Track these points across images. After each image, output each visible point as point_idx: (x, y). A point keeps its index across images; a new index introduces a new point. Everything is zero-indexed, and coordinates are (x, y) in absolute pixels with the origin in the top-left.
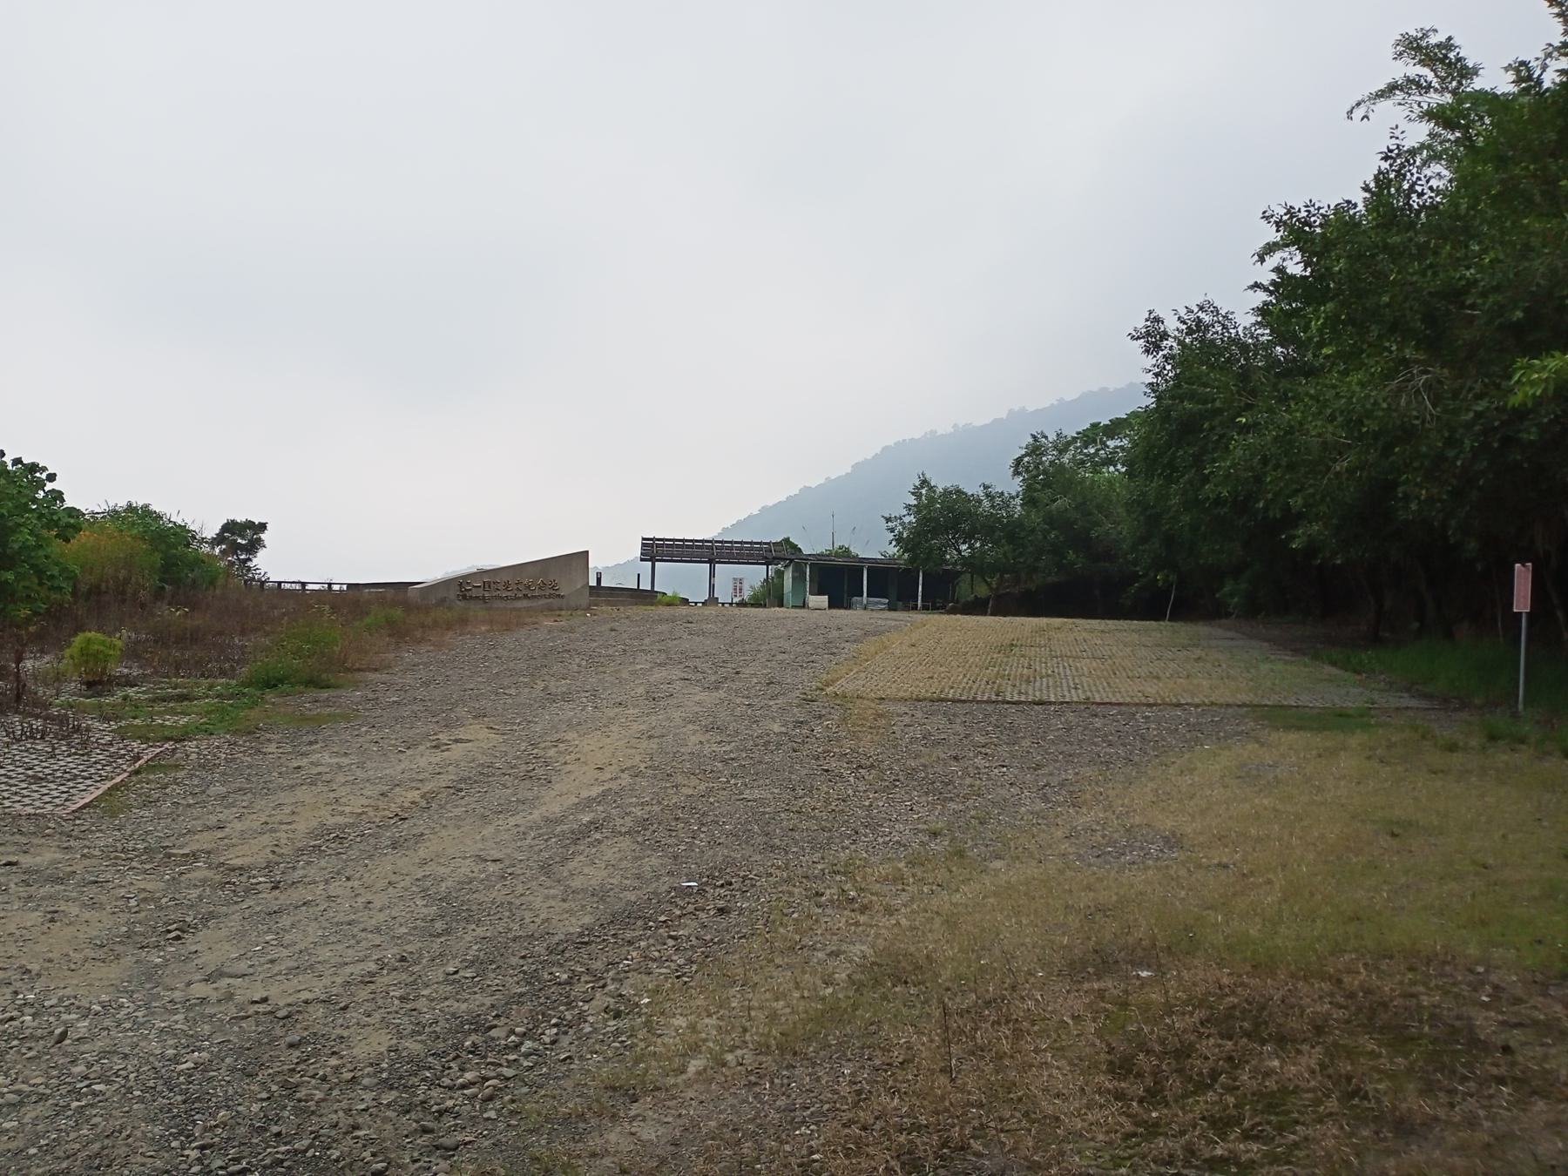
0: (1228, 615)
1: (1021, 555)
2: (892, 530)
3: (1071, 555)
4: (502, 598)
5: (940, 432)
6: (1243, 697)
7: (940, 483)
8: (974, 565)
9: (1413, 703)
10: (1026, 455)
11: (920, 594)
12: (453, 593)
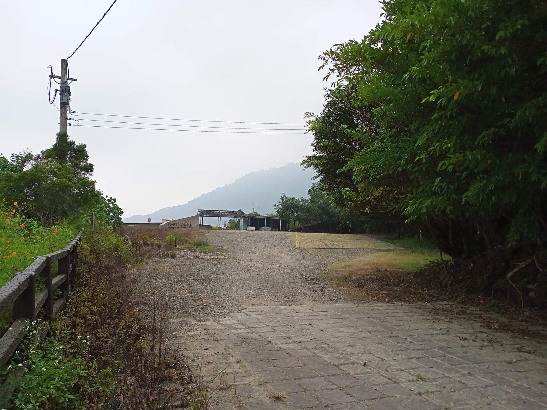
0: (365, 232)
1: (311, 216)
6: (374, 248)
7: (289, 196)
8: (298, 219)
10: (311, 189)
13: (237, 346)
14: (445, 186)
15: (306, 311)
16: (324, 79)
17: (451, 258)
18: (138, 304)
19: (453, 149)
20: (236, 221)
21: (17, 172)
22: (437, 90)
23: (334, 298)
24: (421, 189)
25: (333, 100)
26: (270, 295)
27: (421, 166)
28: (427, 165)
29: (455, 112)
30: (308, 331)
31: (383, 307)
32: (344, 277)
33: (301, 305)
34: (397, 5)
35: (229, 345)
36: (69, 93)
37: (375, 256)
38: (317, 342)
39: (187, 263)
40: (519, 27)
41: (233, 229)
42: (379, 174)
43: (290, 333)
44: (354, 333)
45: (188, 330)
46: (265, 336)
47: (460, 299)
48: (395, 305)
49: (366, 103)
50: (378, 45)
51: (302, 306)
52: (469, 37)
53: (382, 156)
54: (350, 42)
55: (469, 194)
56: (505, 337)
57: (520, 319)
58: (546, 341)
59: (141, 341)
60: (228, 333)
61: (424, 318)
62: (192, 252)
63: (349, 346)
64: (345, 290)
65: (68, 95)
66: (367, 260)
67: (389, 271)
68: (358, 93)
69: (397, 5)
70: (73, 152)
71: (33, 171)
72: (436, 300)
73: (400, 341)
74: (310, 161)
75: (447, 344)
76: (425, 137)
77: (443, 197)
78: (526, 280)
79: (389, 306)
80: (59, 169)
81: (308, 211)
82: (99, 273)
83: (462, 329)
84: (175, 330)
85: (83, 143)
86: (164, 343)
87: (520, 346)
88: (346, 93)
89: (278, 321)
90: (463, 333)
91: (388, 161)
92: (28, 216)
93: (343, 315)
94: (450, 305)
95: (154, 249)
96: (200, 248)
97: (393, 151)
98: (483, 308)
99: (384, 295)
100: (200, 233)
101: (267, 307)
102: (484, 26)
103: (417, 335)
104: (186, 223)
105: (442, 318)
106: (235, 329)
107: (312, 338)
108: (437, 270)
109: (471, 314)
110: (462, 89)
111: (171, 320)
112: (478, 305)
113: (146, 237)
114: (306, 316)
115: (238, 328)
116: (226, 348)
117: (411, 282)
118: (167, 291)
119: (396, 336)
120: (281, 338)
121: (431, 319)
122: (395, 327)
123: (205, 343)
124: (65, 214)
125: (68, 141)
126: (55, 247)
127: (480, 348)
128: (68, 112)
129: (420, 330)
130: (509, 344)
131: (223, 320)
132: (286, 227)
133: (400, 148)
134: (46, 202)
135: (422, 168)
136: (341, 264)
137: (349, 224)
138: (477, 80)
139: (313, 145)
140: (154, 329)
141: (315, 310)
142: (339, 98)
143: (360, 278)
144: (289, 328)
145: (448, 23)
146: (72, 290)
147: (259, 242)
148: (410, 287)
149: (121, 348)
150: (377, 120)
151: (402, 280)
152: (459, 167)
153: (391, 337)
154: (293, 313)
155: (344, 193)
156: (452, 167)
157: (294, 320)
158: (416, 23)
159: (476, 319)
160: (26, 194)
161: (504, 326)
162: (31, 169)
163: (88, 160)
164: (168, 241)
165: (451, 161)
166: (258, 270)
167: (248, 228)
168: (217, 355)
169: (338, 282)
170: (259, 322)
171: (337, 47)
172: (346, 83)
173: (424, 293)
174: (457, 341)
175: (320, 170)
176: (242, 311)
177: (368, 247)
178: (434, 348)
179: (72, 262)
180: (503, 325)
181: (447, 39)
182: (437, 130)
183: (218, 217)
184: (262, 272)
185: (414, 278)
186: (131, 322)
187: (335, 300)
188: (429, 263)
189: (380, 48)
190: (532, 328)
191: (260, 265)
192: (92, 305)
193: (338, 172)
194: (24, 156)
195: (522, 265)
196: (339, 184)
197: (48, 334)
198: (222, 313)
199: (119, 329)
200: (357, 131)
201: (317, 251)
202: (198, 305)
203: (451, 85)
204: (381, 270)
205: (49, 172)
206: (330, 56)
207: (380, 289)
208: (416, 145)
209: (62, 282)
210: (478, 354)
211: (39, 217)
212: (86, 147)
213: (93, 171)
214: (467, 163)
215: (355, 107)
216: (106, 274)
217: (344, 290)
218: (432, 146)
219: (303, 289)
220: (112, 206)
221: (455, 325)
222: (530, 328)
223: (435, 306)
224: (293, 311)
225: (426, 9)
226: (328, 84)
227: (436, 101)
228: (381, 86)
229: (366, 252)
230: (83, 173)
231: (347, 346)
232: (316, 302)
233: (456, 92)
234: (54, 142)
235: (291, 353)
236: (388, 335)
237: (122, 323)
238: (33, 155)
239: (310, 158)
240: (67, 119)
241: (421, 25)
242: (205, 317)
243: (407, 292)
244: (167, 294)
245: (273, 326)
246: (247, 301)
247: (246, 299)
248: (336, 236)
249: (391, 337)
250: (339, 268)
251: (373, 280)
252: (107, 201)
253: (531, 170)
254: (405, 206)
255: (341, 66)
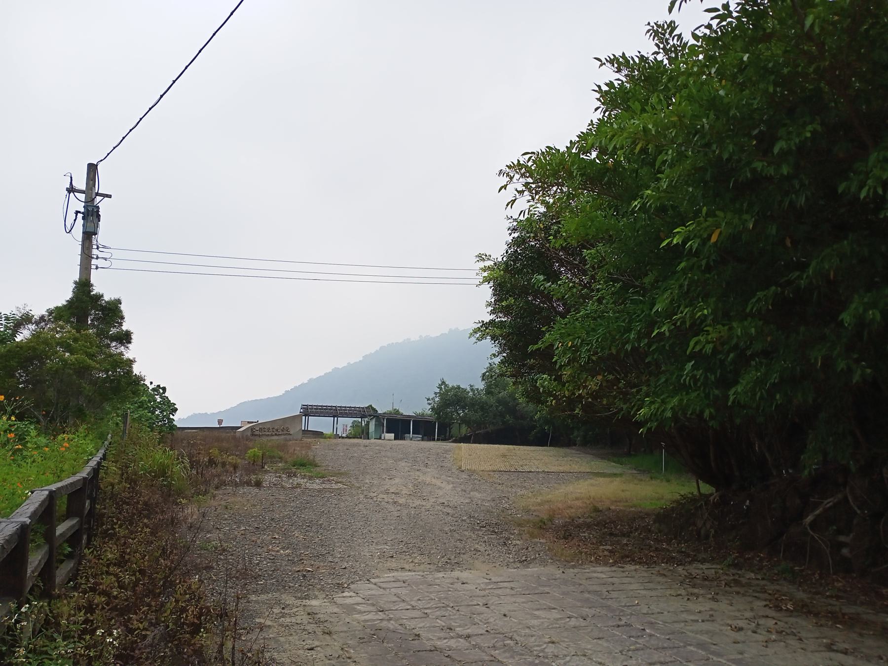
0: (575, 445)
1: (487, 416)
3: (508, 417)
5: (412, 339)
6: (589, 471)
7: (451, 383)
8: (465, 421)
9: (636, 472)
13: (362, 643)
14: (701, 375)
15: (478, 582)
16: (507, 205)
17: (714, 489)
18: (198, 569)
19: (711, 317)
20: (363, 424)
21: (5, 343)
22: (684, 228)
23: (524, 558)
24: (663, 380)
25: (522, 236)
26: (419, 552)
27: (663, 343)
28: (671, 342)
29: (714, 260)
30: (482, 616)
31: (605, 574)
32: (541, 521)
33: (470, 571)
34: (621, 96)
35: (350, 642)
36: (98, 216)
37: (592, 485)
38: (499, 635)
39: (280, 497)
40: (808, 135)
41: (358, 438)
42: (596, 353)
43: (452, 619)
44: (557, 619)
45: (281, 615)
46: (409, 626)
47: (729, 560)
48: (625, 569)
49: (574, 243)
50: (591, 154)
51: (472, 572)
52: (733, 148)
53: (600, 325)
54: (548, 150)
55: (739, 390)
56: (805, 625)
57: (827, 594)
58: (871, 633)
59: (203, 636)
60: (347, 620)
61: (672, 592)
62: (289, 477)
63: (550, 642)
64: (543, 543)
65: (96, 220)
66: (579, 491)
67: (613, 511)
68: (561, 226)
69: (621, 96)
70: (99, 311)
71: (32, 342)
72: (692, 560)
73: (634, 634)
74: (485, 330)
75: (710, 639)
76: (667, 298)
77: (698, 392)
78: (835, 528)
79: (615, 571)
80: (76, 340)
81: (482, 408)
82: (134, 514)
83: (735, 611)
84: (260, 615)
85: (117, 297)
86: (239, 639)
87: (829, 641)
88: (541, 225)
89: (432, 599)
90: (736, 618)
91: (610, 334)
92: (20, 418)
93: (540, 588)
94: (713, 570)
95: (227, 471)
96: (303, 471)
97: (617, 318)
98: (768, 574)
99: (606, 553)
100: (304, 445)
101: (413, 573)
102: (755, 132)
103: (660, 623)
104: (280, 428)
105: (702, 592)
106: (360, 612)
107: (489, 629)
108: (692, 510)
109: (749, 585)
110: (723, 227)
111: (253, 597)
112: (760, 569)
113: (215, 451)
114: (478, 590)
115: (365, 612)
116: (345, 646)
117: (650, 531)
118: (247, 546)
119: (628, 625)
120: (436, 629)
121: (683, 594)
122: (625, 609)
123: (309, 638)
124: (80, 414)
125: (92, 293)
126: (63, 471)
127: (764, 644)
128: (95, 247)
129: (666, 613)
130: (811, 638)
131: (339, 597)
132: (445, 436)
133: (628, 313)
134: (51, 393)
135: (664, 346)
136: (537, 499)
137: (549, 430)
138: (747, 212)
139: (489, 305)
140: (223, 615)
141: (494, 579)
142: (531, 232)
143: (567, 522)
144: (450, 611)
145: (699, 127)
146: (88, 547)
147: (401, 460)
148: (648, 539)
149: (168, 647)
150: (590, 269)
151: (636, 527)
152: (723, 344)
153: (619, 626)
154: (456, 584)
155: (540, 384)
156: (711, 346)
157: (458, 597)
158: (650, 126)
159: (757, 595)
160: (18, 379)
161: (803, 606)
162: (30, 339)
163: (124, 324)
164: (249, 457)
165: (710, 337)
166: (399, 508)
167: (383, 435)
168: (329, 659)
169: (531, 530)
170: (399, 600)
171: (527, 157)
172: (542, 209)
173: (671, 549)
174: (727, 633)
175: (500, 345)
176: (372, 580)
177: (580, 470)
178: (690, 645)
179: (90, 497)
180: (800, 604)
181: (699, 152)
182: (686, 287)
183: (334, 417)
184: (405, 512)
185: (655, 522)
186: (185, 602)
187: (526, 560)
188: (679, 497)
189: (594, 158)
190: (850, 610)
191: (402, 501)
192: (120, 572)
193: (530, 349)
194: (18, 317)
195: (829, 502)
196: (531, 368)
197: (47, 622)
198: (338, 584)
199: (166, 615)
200: (560, 285)
201: (497, 476)
202: (299, 571)
203: (706, 221)
204: (601, 508)
205: (58, 344)
206: (518, 170)
207: (600, 542)
208: (654, 310)
209: (72, 532)
210: (762, 656)
211: (37, 418)
212: (121, 304)
213: (130, 343)
214: (735, 341)
215: (557, 247)
216: (145, 517)
217: (540, 543)
218: (679, 312)
219: (474, 542)
220: (159, 400)
221: (723, 605)
222: (846, 610)
223: (689, 571)
224: (456, 581)
225: (664, 103)
226: (514, 212)
227: (684, 242)
228: (597, 217)
229: (576, 477)
230: (114, 345)
231: (545, 643)
232: (494, 565)
233: (714, 230)
234: (69, 295)
235: (454, 656)
236: (615, 624)
237: (170, 606)
238: (33, 316)
239: (485, 325)
240: (93, 258)
241: (658, 129)
242: (310, 592)
243: (644, 547)
244: (247, 552)
245: (422, 609)
246: (381, 564)
247: (378, 560)
248: (528, 451)
249: (619, 626)
250: (533, 505)
251: (588, 526)
252: (151, 390)
253: (835, 353)
254: (638, 406)
255: (533, 186)
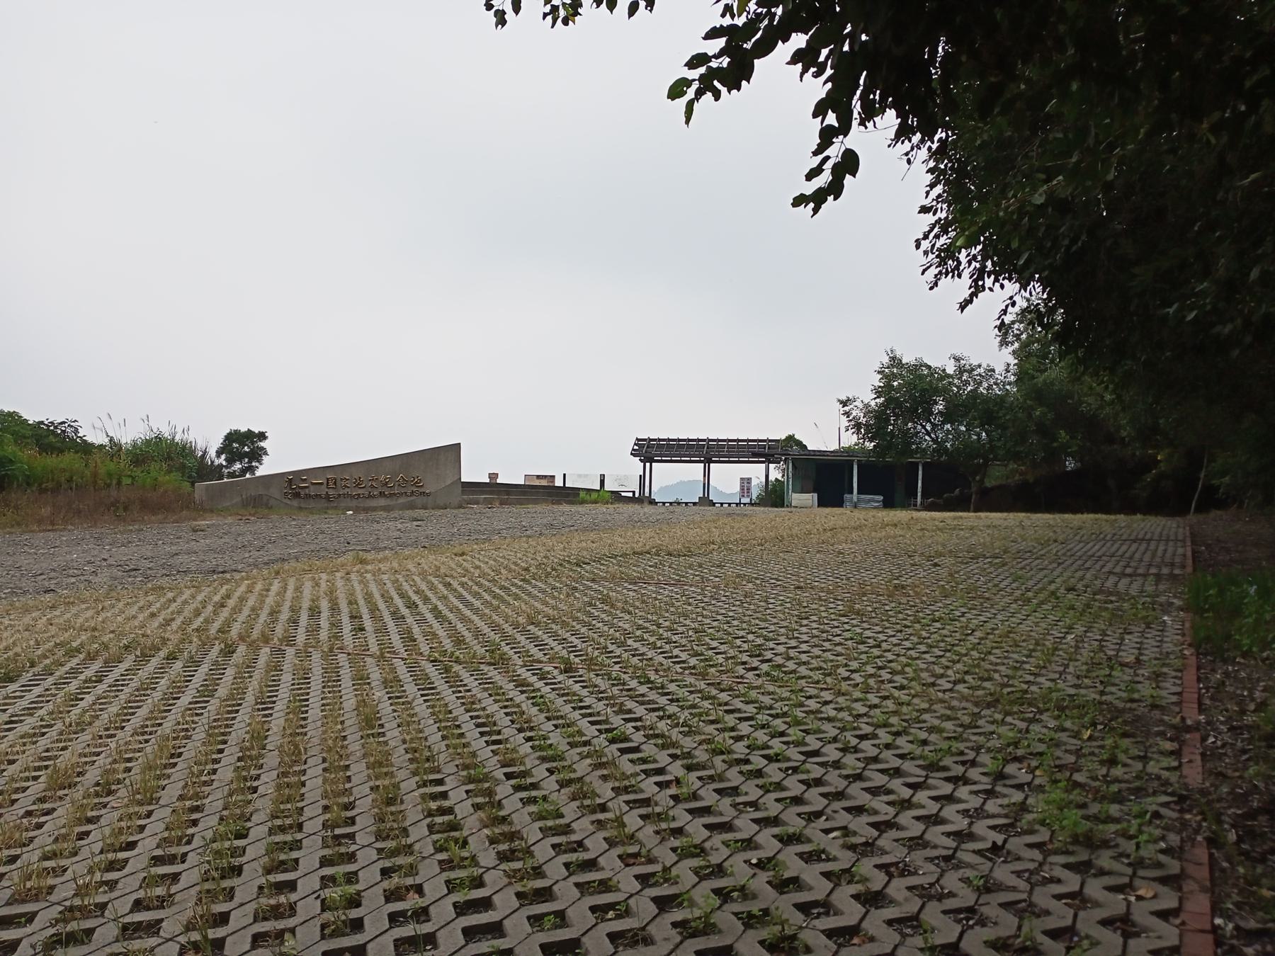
2: (847, 414)
4: (352, 497)
11: (919, 489)
12: (275, 492)
